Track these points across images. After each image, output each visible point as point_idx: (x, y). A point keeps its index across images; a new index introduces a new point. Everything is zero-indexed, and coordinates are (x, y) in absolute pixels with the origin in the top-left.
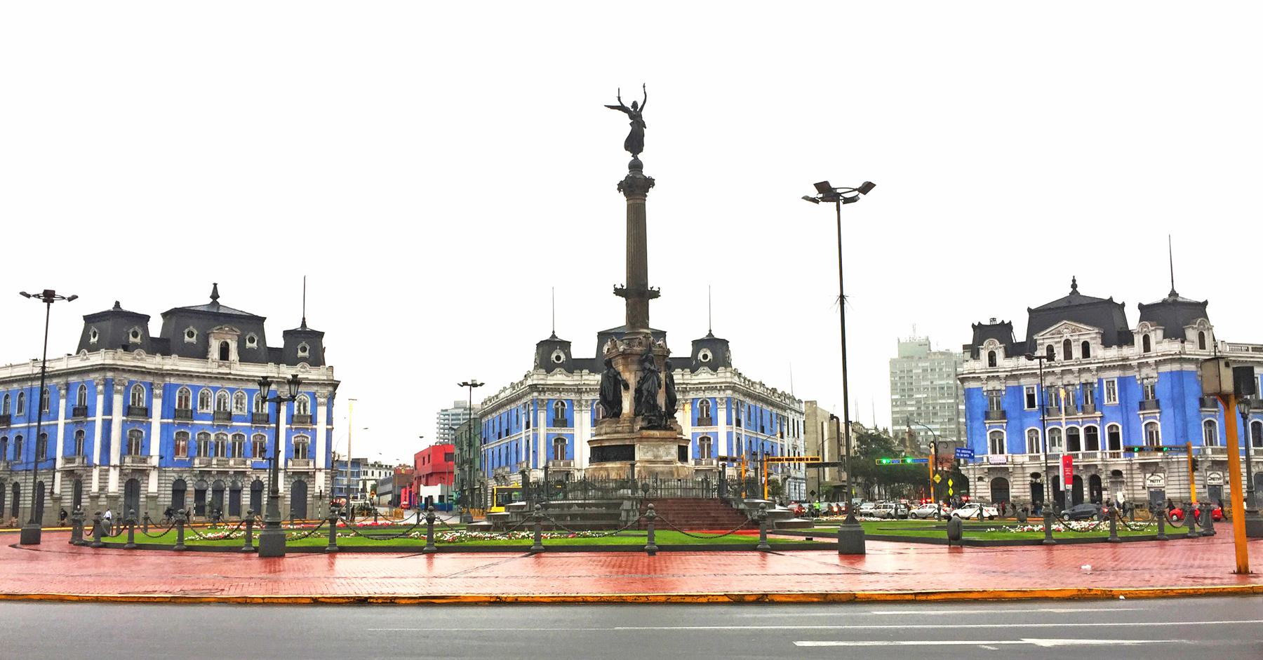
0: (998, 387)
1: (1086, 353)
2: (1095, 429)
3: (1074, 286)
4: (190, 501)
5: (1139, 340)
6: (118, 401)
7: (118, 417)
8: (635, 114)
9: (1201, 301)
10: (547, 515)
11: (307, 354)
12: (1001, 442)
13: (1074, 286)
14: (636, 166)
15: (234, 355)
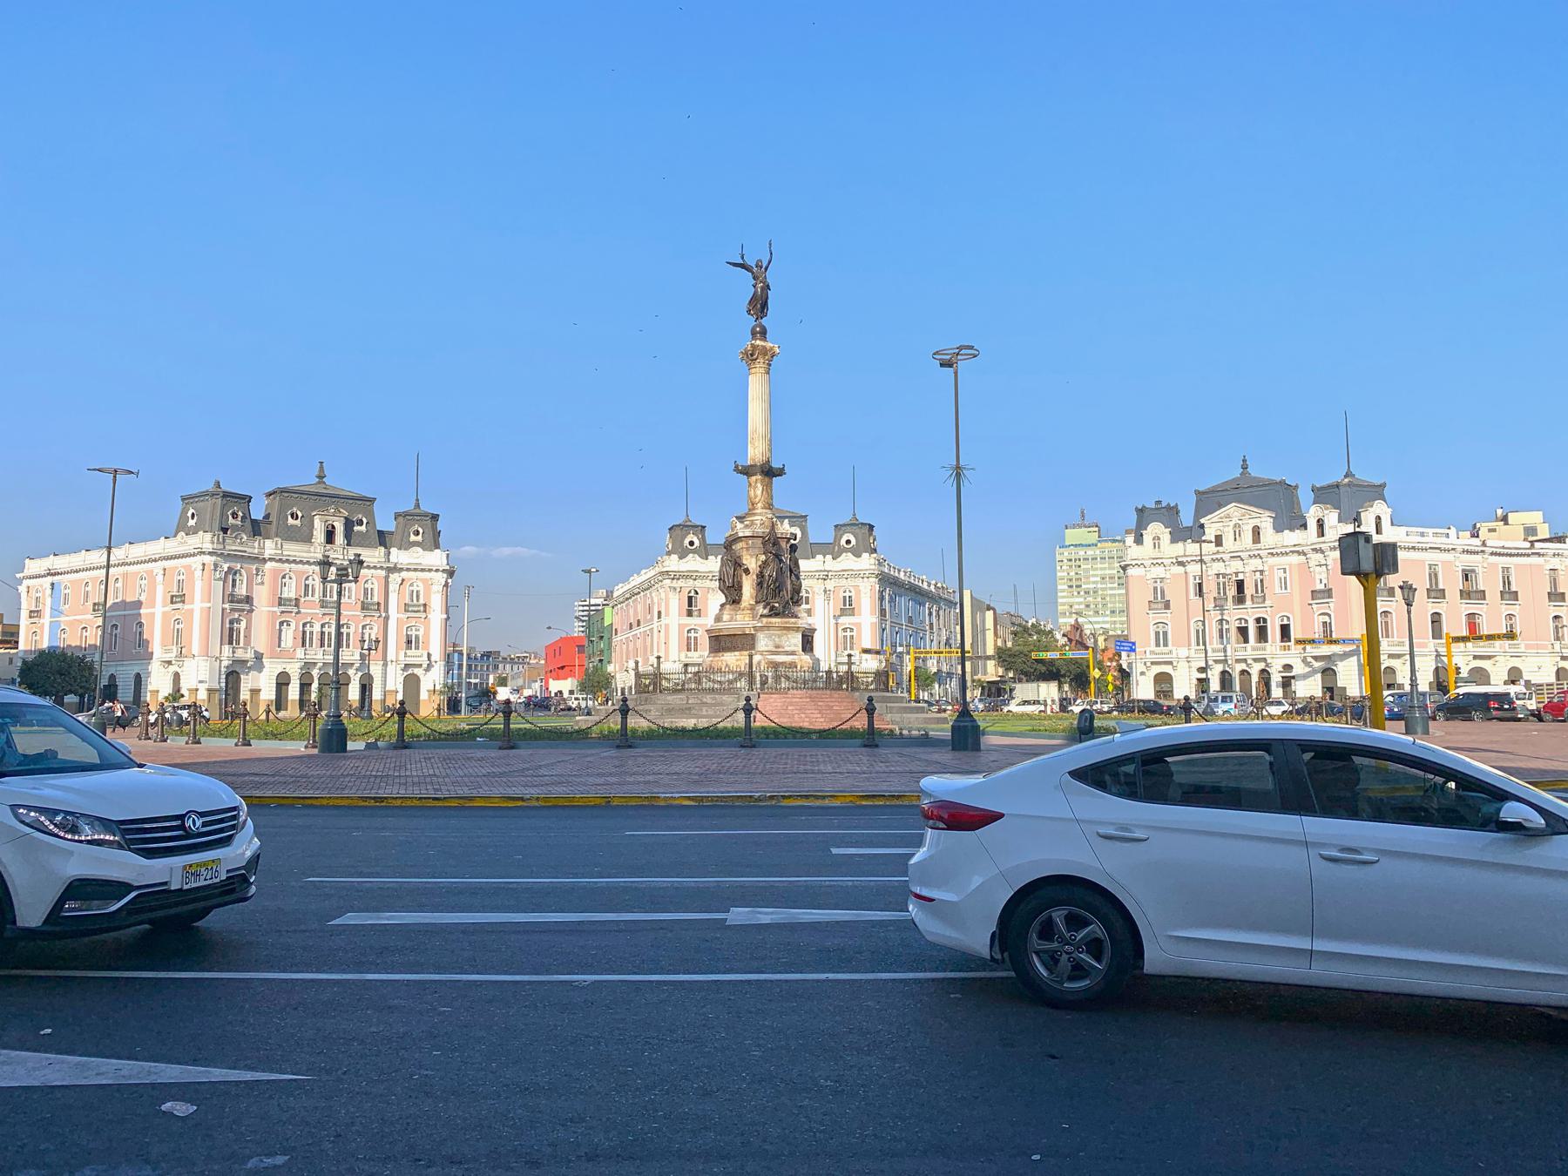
2: (1265, 620)
3: (1245, 467)
8: (758, 272)
10: (395, 748)
11: (419, 538)
13: (1245, 467)
15: (339, 538)
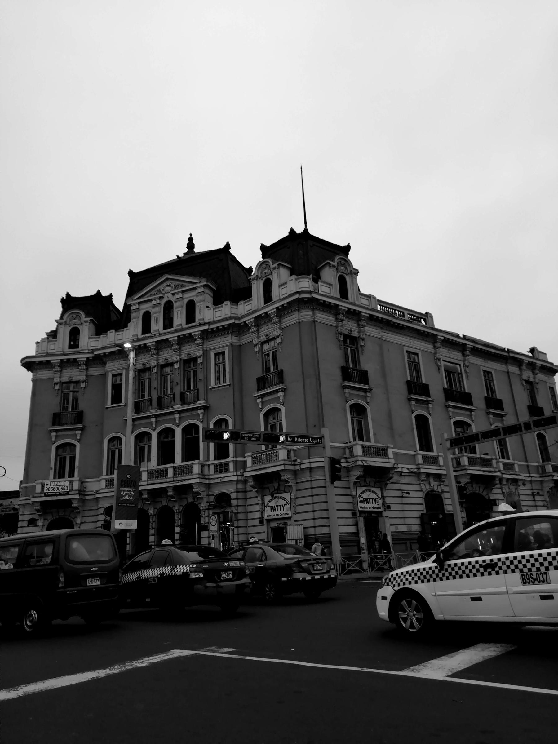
0: (76, 378)
1: (190, 317)
4: (240, 478)
5: (258, 289)
9: (343, 244)
12: (73, 459)
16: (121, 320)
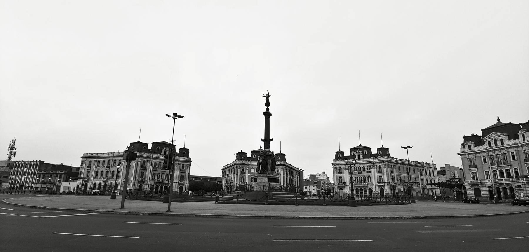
1: (502, 143)
3: (499, 120)
6: (239, 170)
7: (239, 174)
12: (476, 175)
13: (499, 120)
14: (268, 109)
16: (482, 143)
